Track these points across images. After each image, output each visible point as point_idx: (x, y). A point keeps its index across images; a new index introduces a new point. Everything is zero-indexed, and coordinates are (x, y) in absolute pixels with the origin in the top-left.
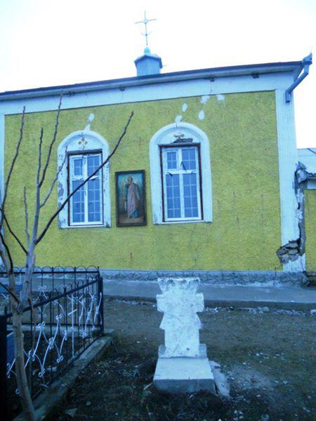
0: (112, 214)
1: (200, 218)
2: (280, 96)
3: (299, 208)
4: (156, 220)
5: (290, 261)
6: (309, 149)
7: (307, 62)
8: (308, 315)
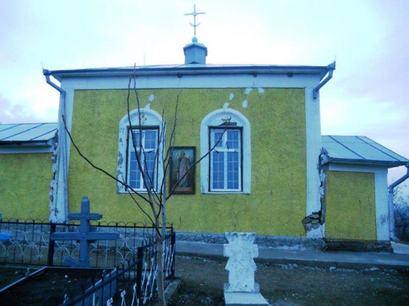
1: (240, 189)
2: (309, 93)
3: (321, 186)
4: (204, 190)
5: (312, 229)
6: (329, 136)
7: (331, 68)
8: (328, 271)
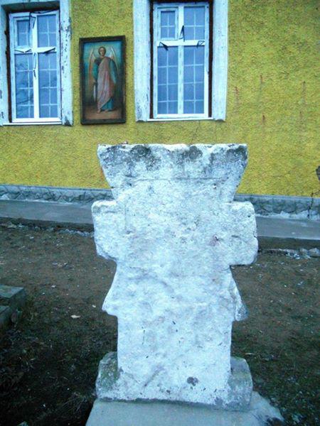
0: (74, 105)
1: (205, 116)
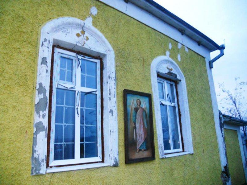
0: (119, 146)
